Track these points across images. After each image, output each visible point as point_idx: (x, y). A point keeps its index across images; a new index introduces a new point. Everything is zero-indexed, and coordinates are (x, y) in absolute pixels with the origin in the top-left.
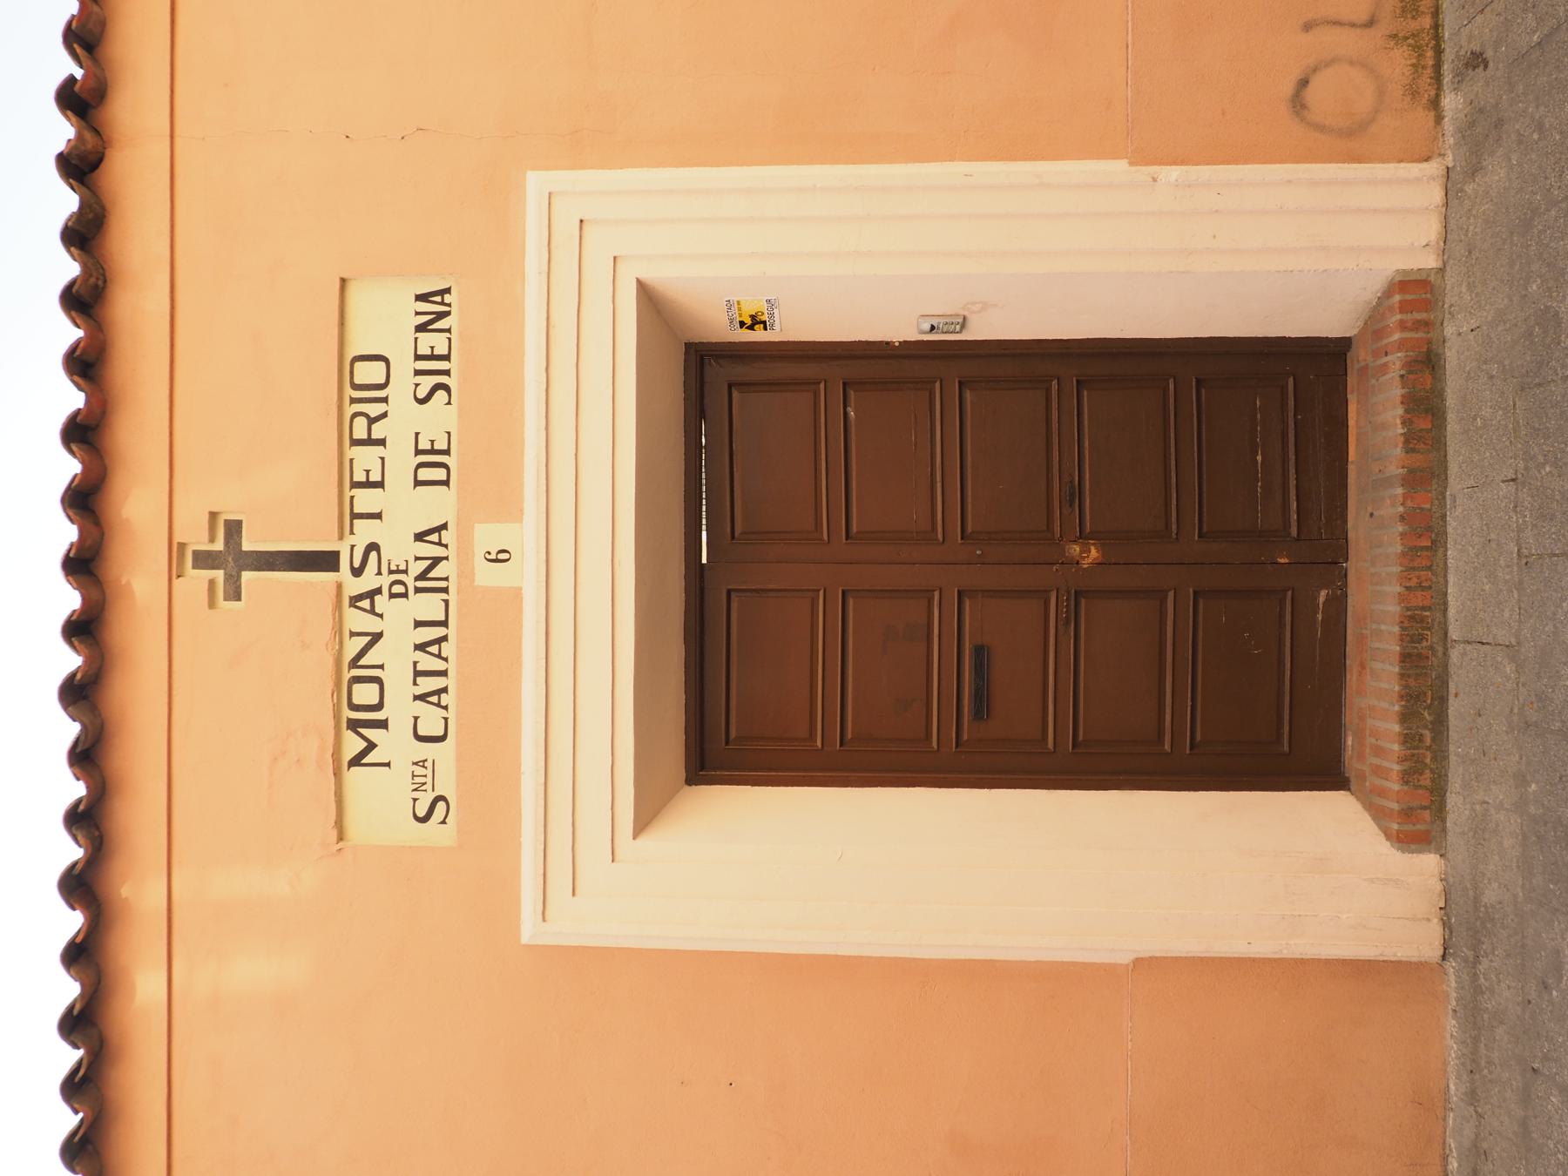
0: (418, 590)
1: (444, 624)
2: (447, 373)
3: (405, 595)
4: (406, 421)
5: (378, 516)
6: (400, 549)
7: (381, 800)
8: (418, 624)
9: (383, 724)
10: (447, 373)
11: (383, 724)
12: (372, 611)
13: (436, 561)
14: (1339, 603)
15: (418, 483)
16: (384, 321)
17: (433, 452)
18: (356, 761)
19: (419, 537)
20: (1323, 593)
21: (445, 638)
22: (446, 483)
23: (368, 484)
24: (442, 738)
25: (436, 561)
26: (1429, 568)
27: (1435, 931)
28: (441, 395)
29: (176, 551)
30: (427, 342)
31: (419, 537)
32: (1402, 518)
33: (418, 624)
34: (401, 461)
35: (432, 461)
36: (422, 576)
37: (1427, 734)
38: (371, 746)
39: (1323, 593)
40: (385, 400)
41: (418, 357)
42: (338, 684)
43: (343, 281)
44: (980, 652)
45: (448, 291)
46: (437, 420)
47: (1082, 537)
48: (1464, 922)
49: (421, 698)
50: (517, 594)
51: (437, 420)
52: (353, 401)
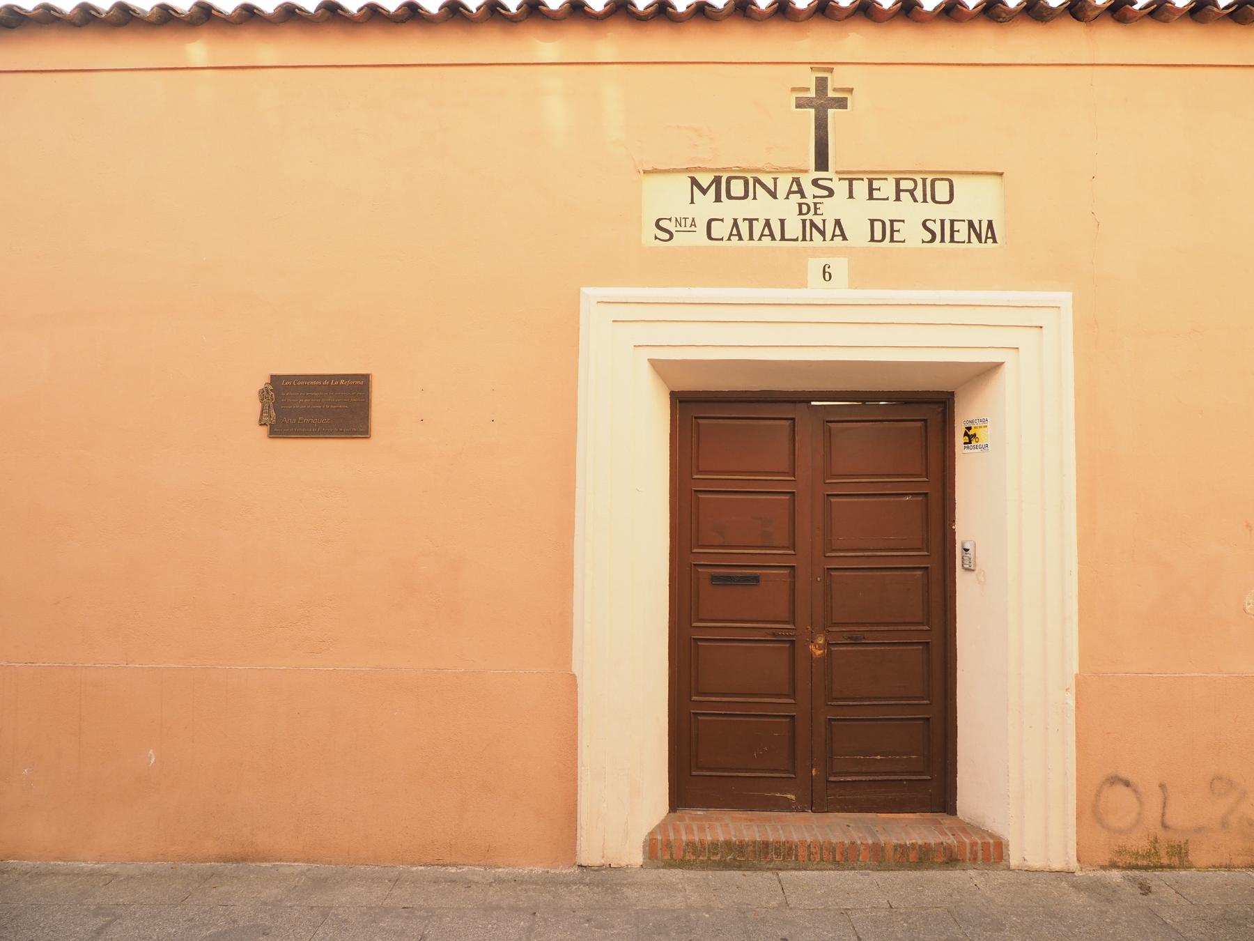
0: (804, 221)
1: (783, 238)
2: (943, 240)
3: (801, 213)
4: (912, 213)
5: (851, 196)
6: (830, 210)
7: (669, 197)
8: (782, 221)
9: (718, 199)
10: (943, 240)
11: (718, 199)
12: (790, 192)
13: (823, 233)
14: (787, 807)
15: (872, 221)
16: (975, 200)
17: (892, 231)
18: (694, 182)
19: (838, 222)
20: (793, 797)
21: (773, 239)
22: (872, 240)
23: (871, 190)
24: (710, 237)
25: (823, 233)
26: (822, 860)
27: (596, 860)
28: (928, 236)
29: (829, 67)
30: (962, 228)
31: (838, 222)
32: (853, 843)
33: (782, 221)
34: (887, 210)
35: (887, 230)
36: (813, 224)
37: (717, 858)
38: (704, 191)
39: (793, 797)
40: (925, 201)
41: (952, 222)
42: (744, 170)
43: (1001, 174)
44: (756, 579)
45: (995, 241)
46: (912, 234)
47: (828, 644)
48: (604, 877)
49: (735, 224)
50: (804, 285)
51: (912, 234)
52: (924, 180)
